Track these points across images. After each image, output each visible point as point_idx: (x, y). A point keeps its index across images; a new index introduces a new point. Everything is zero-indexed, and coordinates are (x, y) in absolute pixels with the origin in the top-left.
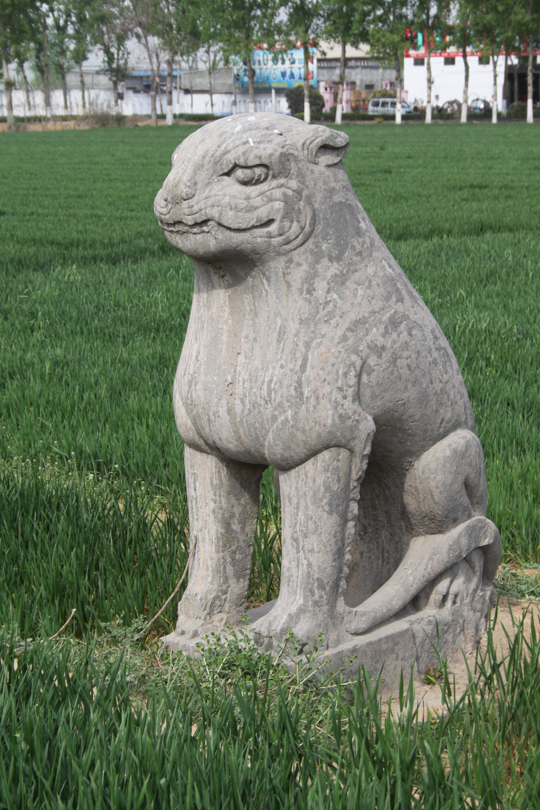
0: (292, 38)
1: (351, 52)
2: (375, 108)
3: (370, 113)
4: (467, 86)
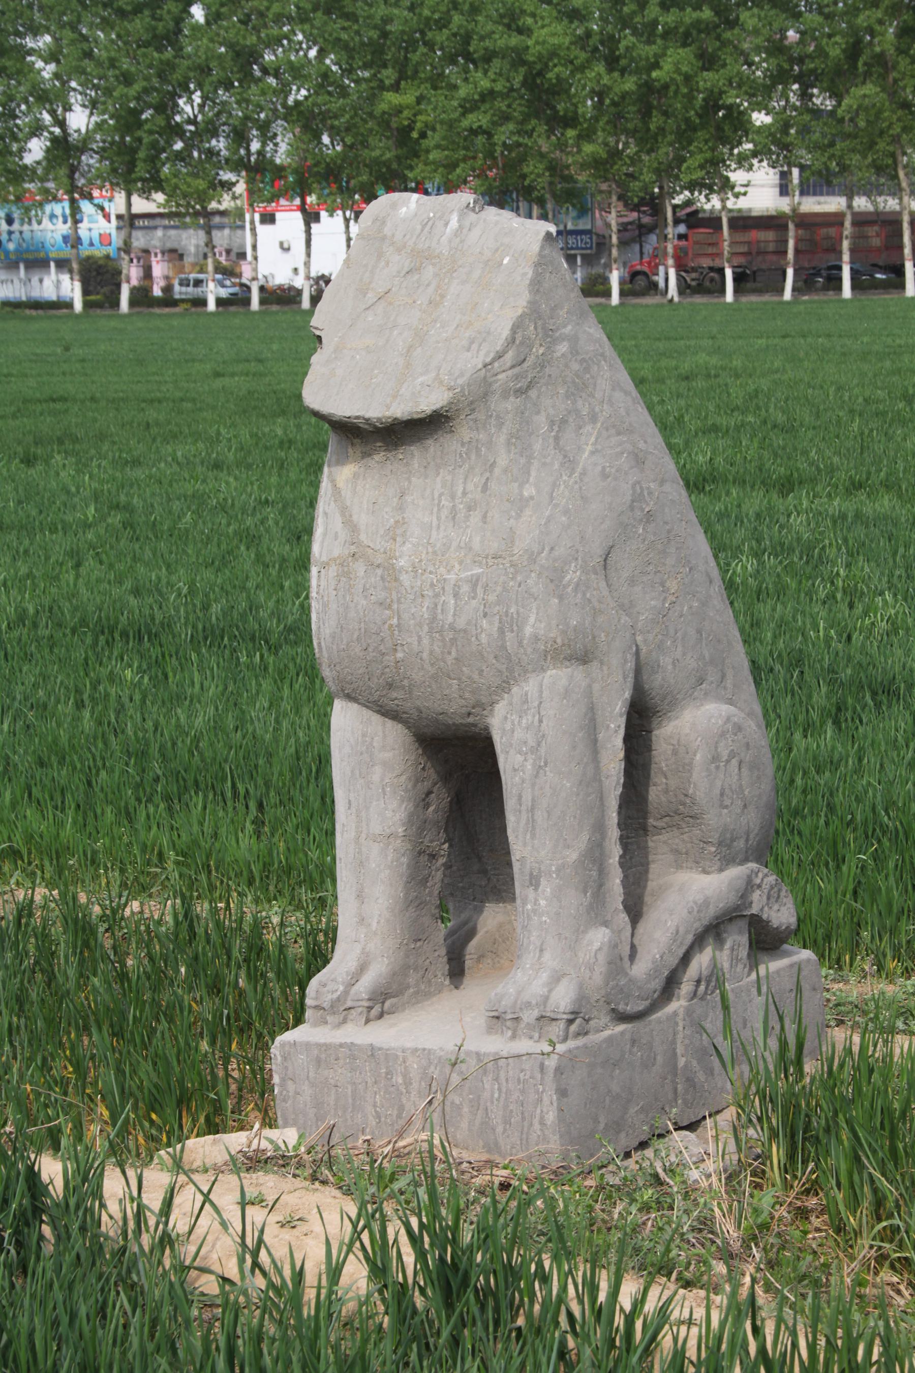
0: (51, 185)
1: (140, 205)
2: (184, 289)
3: (177, 296)
4: (308, 255)
